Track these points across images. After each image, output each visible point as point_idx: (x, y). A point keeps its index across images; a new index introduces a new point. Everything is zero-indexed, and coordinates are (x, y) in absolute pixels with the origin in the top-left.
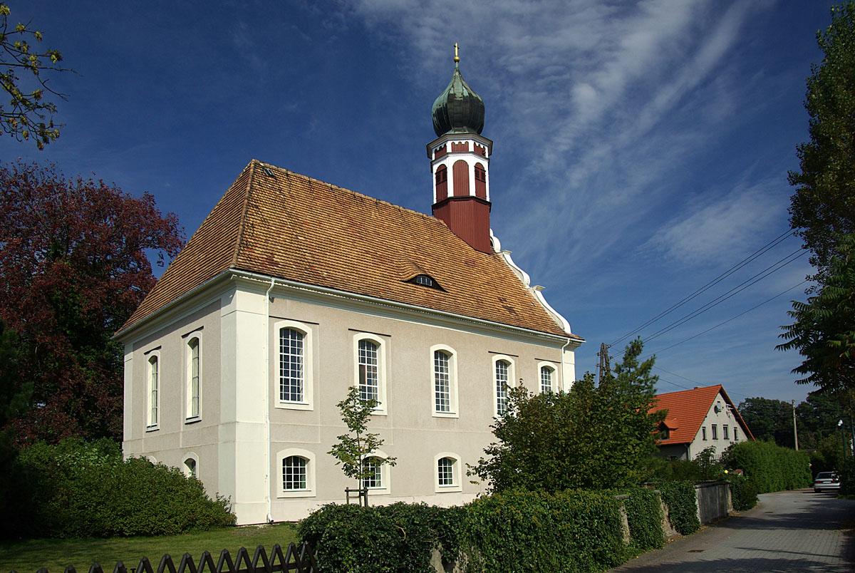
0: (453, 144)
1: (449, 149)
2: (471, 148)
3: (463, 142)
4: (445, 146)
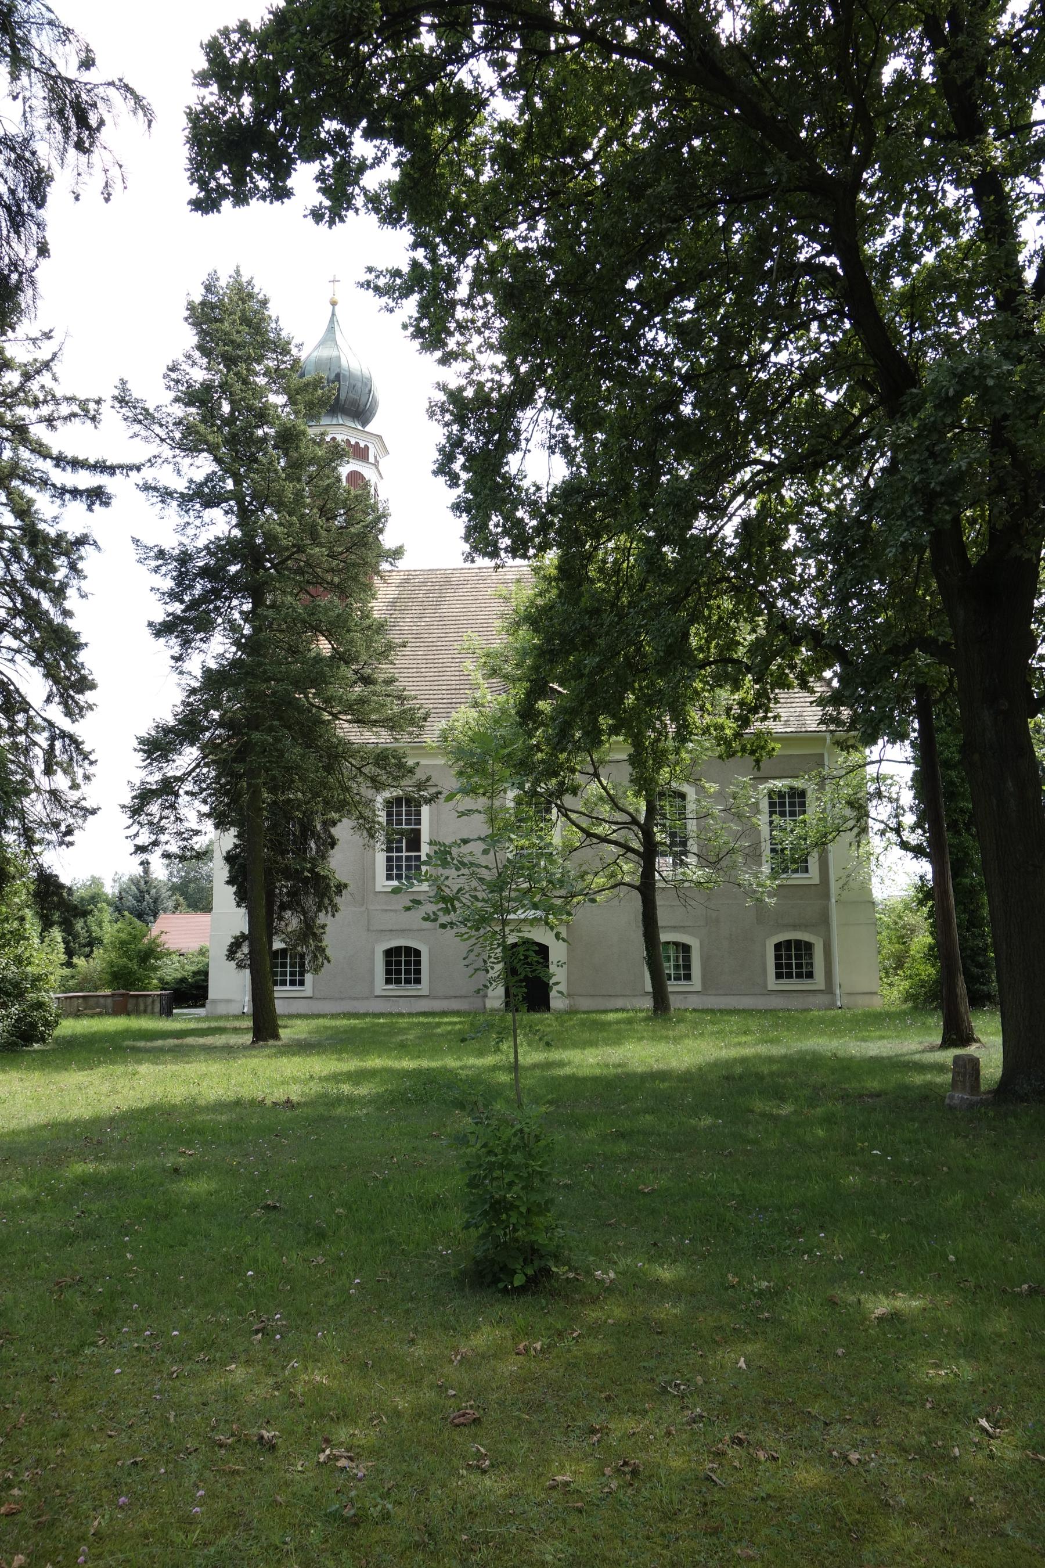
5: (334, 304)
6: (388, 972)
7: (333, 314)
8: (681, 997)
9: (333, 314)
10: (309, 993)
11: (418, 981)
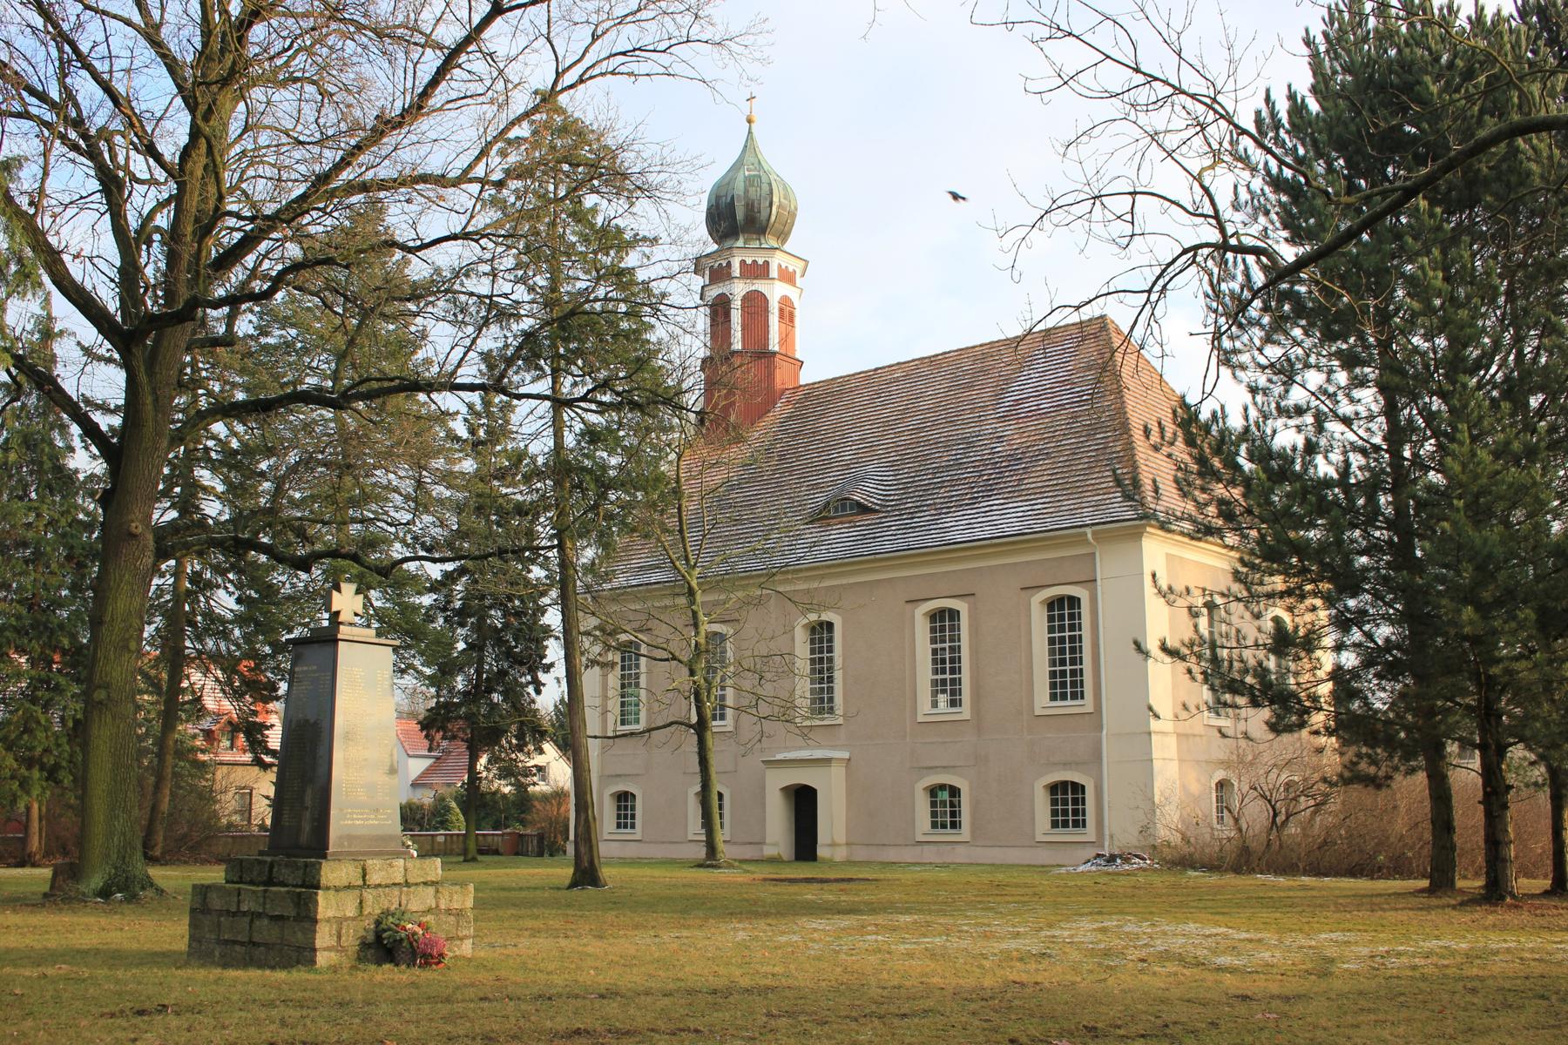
0: (743, 262)
1: (736, 270)
2: (774, 273)
3: (760, 262)
4: (729, 264)
5: (749, 121)
6: (1054, 813)
7: (750, 132)
8: (949, 847)
9: (750, 132)
10: (638, 837)
11: (633, 826)
